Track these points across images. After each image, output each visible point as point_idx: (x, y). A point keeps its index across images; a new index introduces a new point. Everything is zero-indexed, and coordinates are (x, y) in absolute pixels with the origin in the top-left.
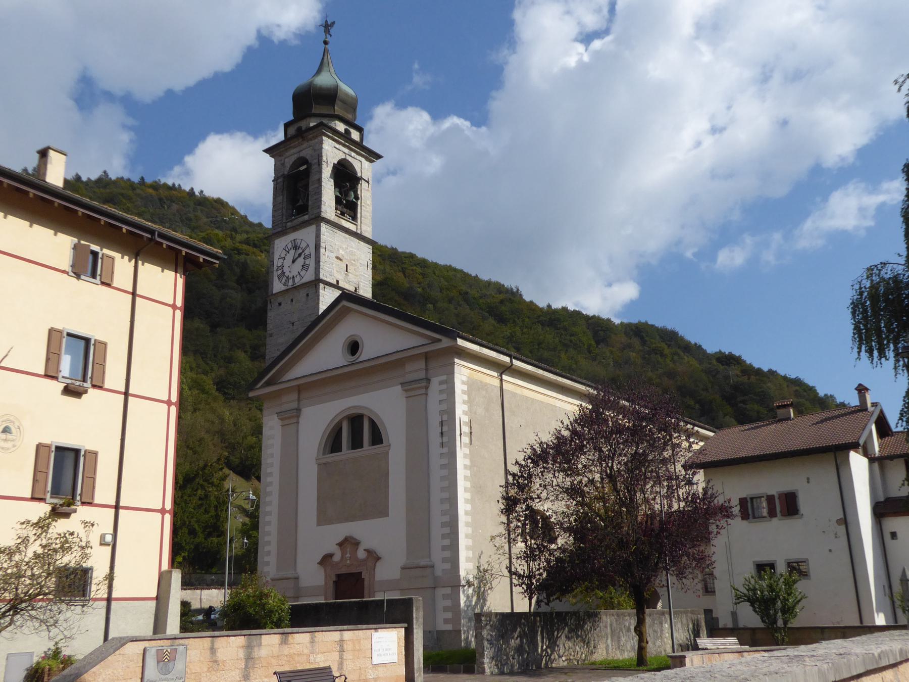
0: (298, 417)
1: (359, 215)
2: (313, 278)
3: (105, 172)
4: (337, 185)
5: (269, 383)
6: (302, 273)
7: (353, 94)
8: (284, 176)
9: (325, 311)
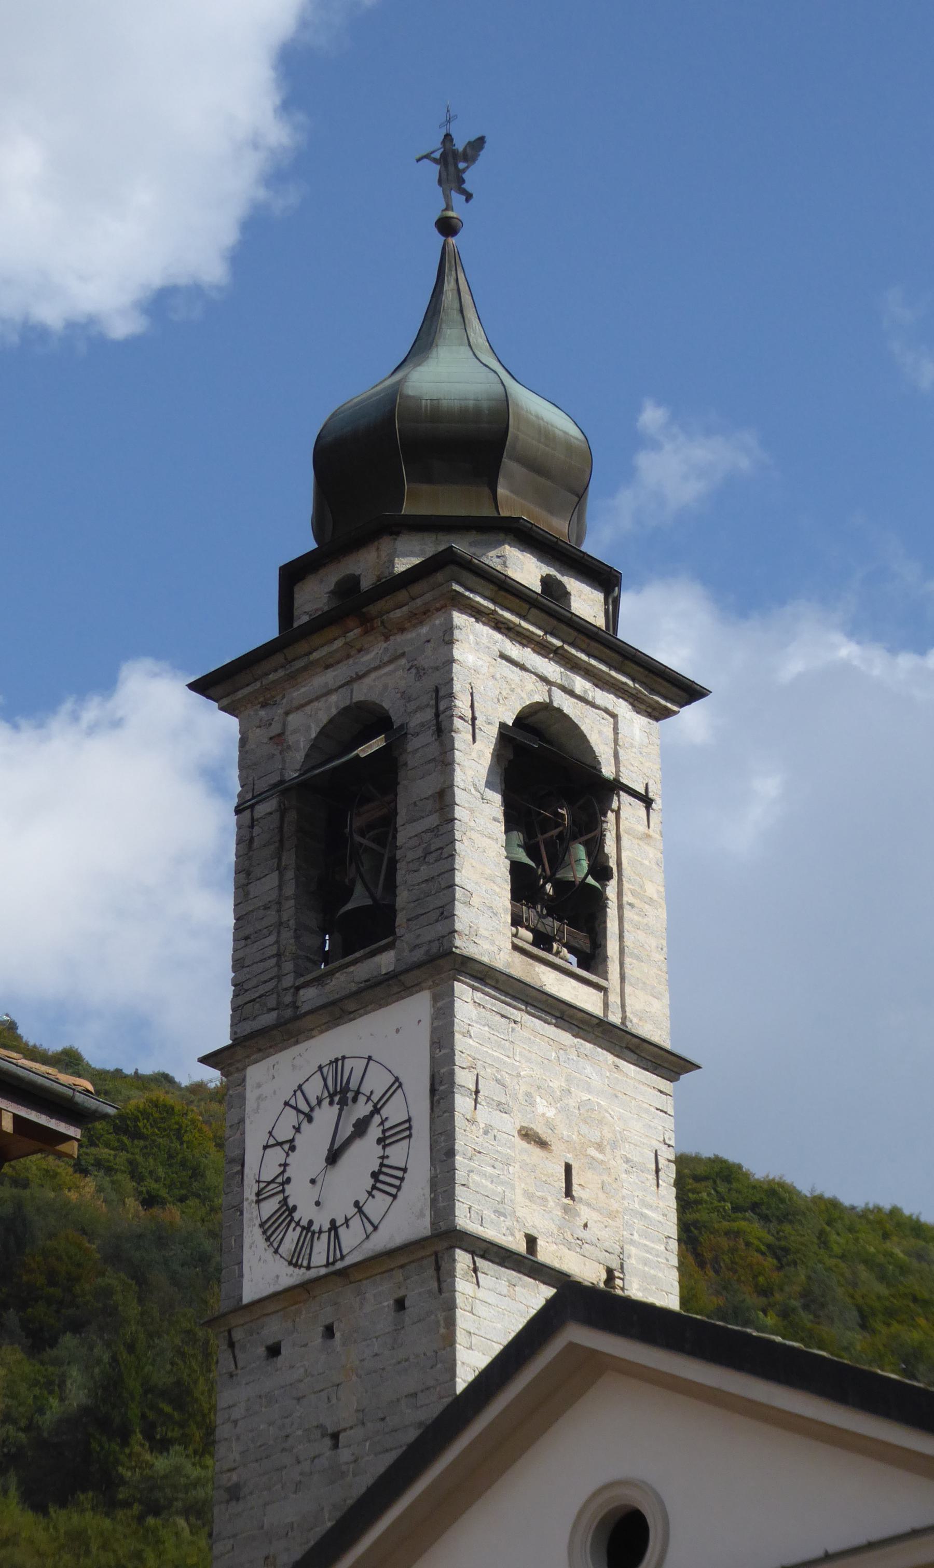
2: (423, 1227)
4: (515, 818)
6: (376, 1206)
7: (573, 431)
8: (283, 789)
9: (474, 1386)
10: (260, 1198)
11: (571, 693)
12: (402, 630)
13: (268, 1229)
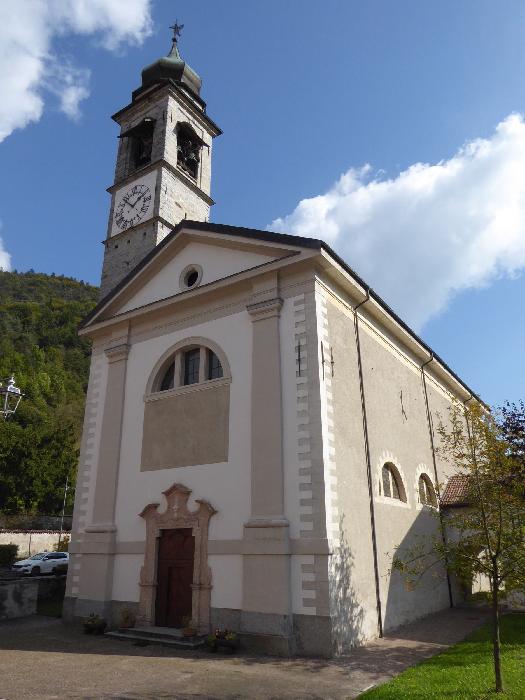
0: (127, 353)
1: (199, 175)
3: (32, 269)
5: (98, 321)
10: (117, 216)
11: (194, 123)
12: (157, 101)
13: (118, 223)
